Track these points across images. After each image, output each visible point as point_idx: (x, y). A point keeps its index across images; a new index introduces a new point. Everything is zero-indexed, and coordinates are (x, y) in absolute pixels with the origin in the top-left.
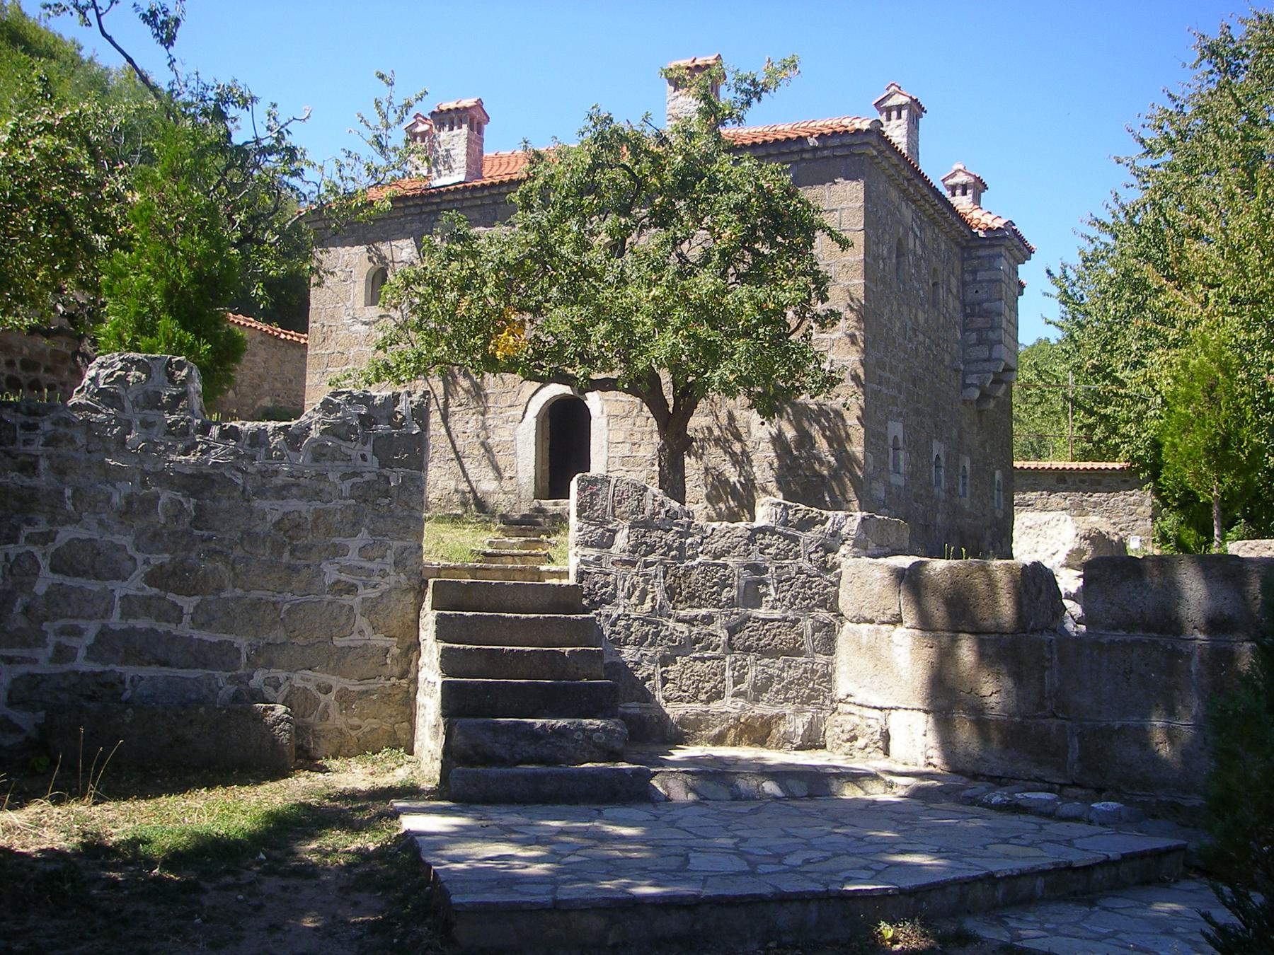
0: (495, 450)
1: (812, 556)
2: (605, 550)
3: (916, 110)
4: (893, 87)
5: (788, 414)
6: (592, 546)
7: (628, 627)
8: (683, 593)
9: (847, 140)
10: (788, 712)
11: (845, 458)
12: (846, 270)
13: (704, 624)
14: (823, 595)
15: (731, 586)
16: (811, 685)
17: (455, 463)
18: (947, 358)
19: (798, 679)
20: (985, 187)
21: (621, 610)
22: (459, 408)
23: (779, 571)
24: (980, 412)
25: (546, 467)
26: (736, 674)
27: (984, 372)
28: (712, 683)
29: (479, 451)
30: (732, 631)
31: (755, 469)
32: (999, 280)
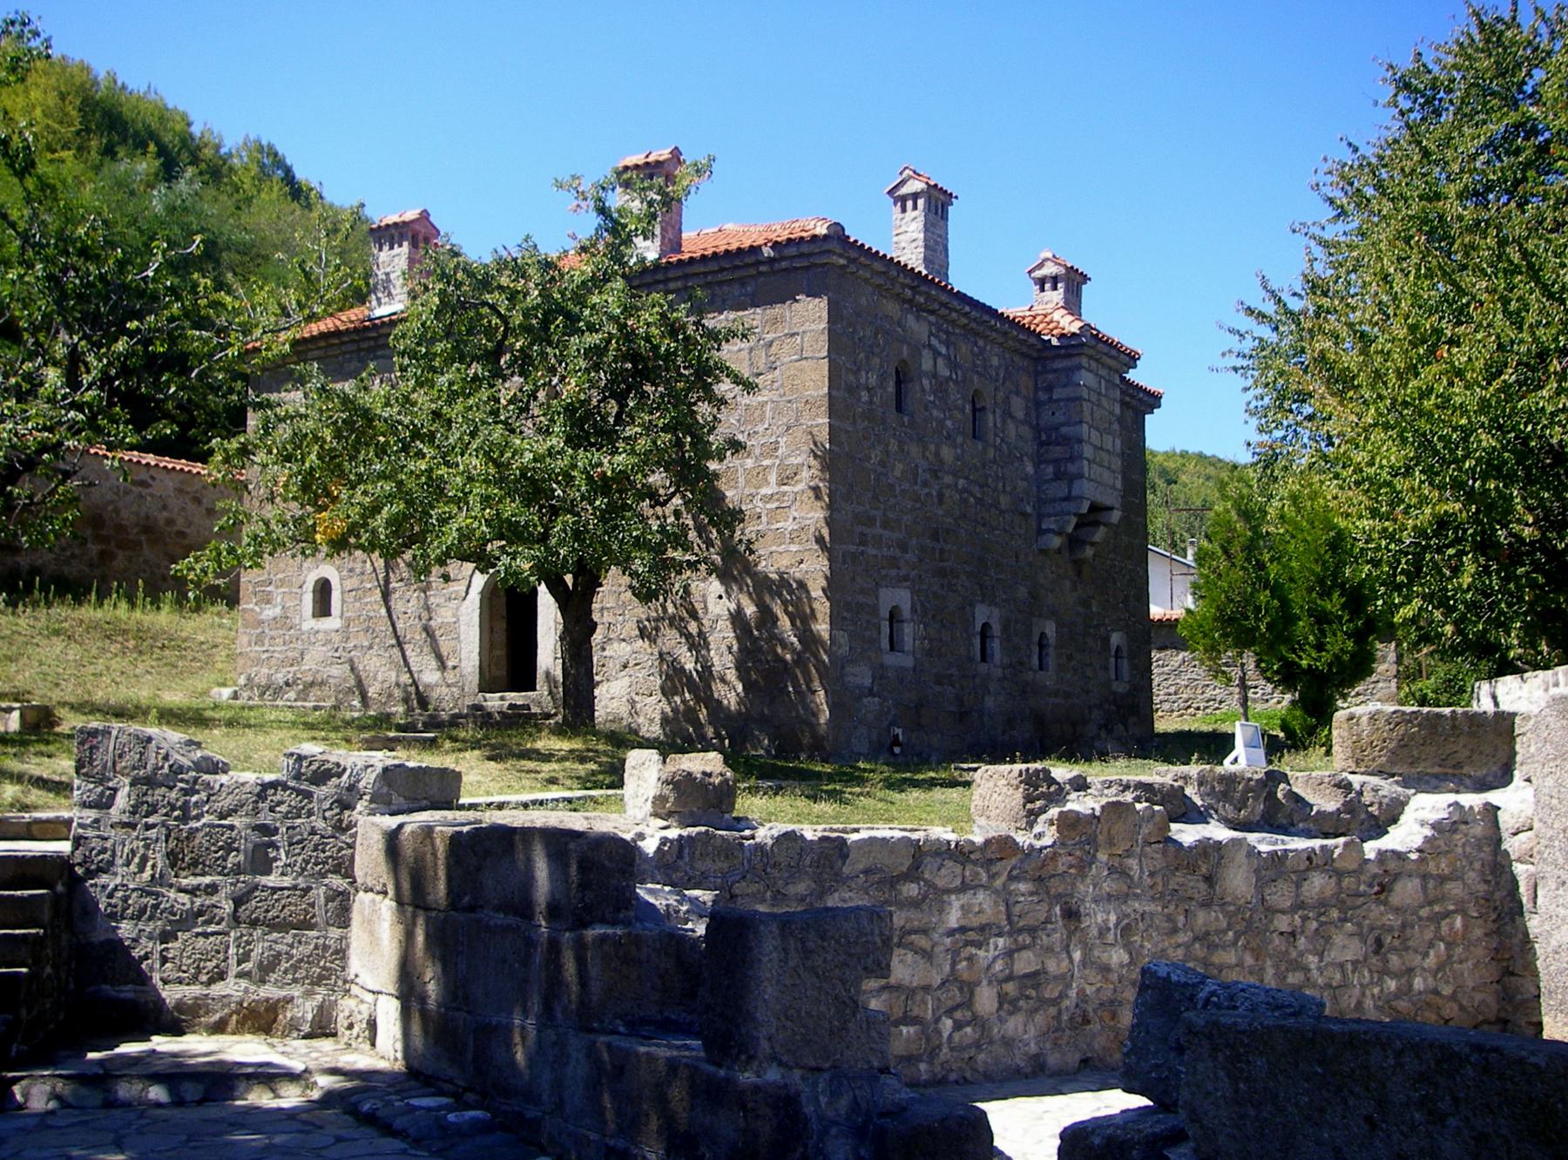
0: (438, 633)
1: (328, 814)
2: (104, 811)
3: (938, 203)
4: (907, 171)
5: (748, 586)
6: (90, 807)
7: (125, 899)
8: (187, 859)
9: (805, 249)
10: (296, 994)
11: (809, 639)
12: (808, 406)
13: (207, 894)
14: (337, 859)
15: (237, 850)
16: (322, 963)
17: (396, 651)
18: (1004, 501)
19: (308, 957)
20: (1085, 278)
21: (118, 880)
22: (400, 584)
23: (290, 831)
24: (1078, 564)
25: (501, 652)
26: (241, 951)
27: (1063, 513)
28: (215, 962)
29: (420, 637)
30: (238, 901)
31: (712, 653)
32: (1079, 399)
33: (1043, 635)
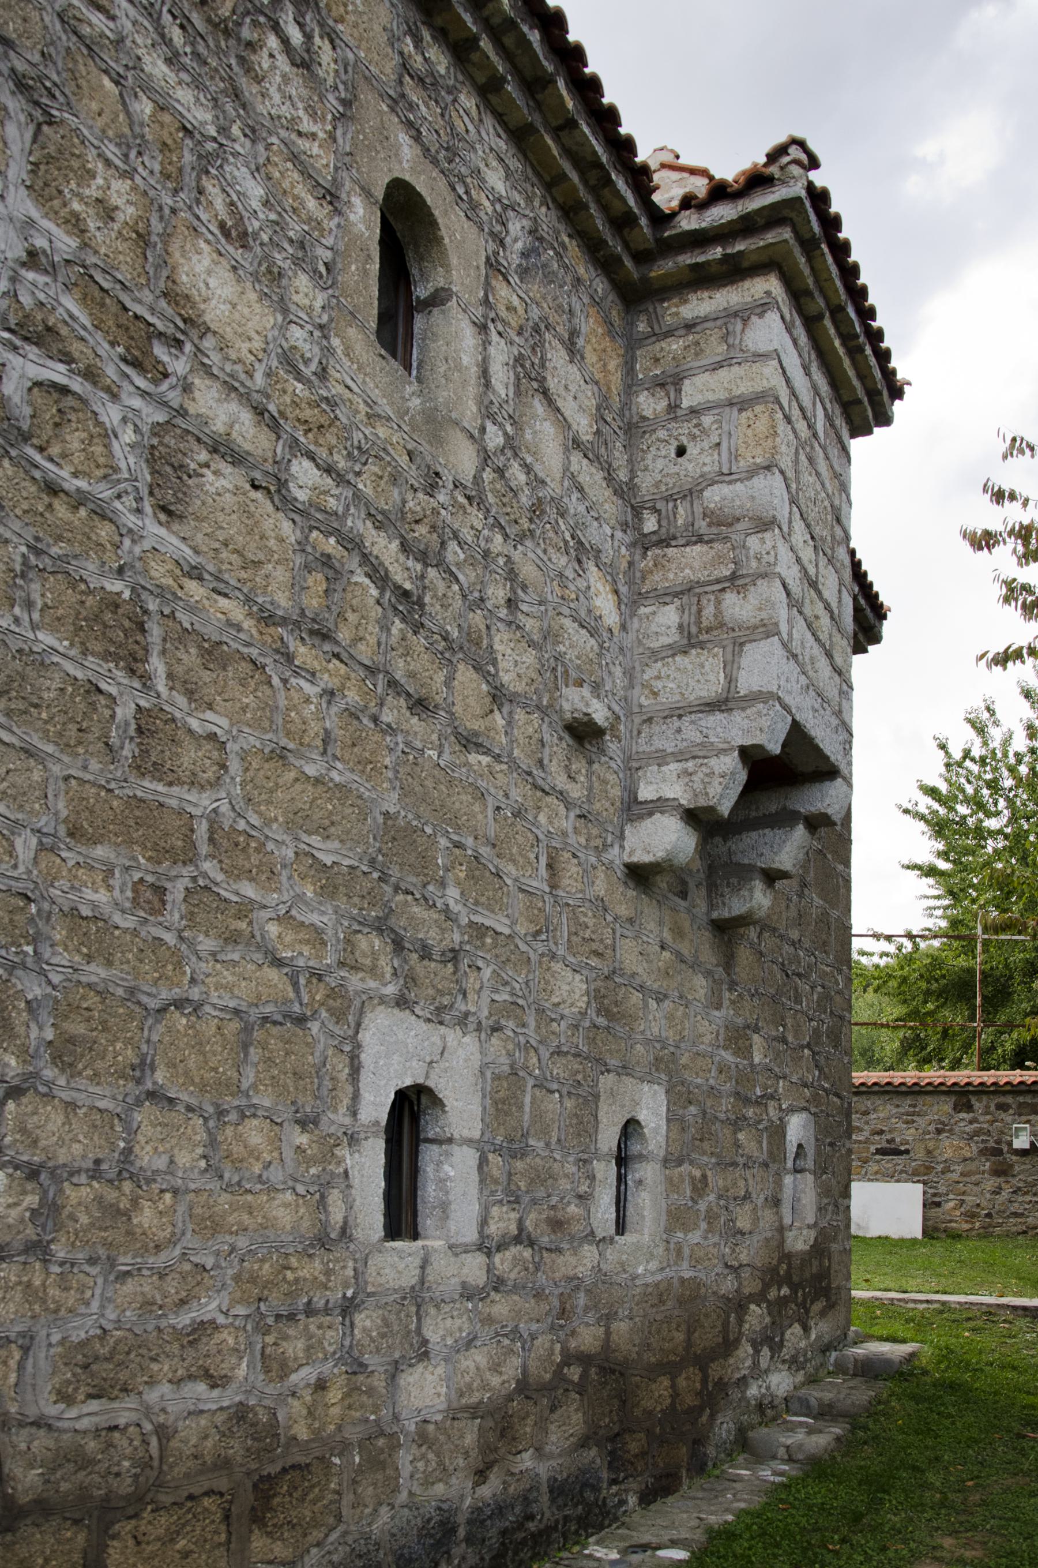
33: (631, 1128)
